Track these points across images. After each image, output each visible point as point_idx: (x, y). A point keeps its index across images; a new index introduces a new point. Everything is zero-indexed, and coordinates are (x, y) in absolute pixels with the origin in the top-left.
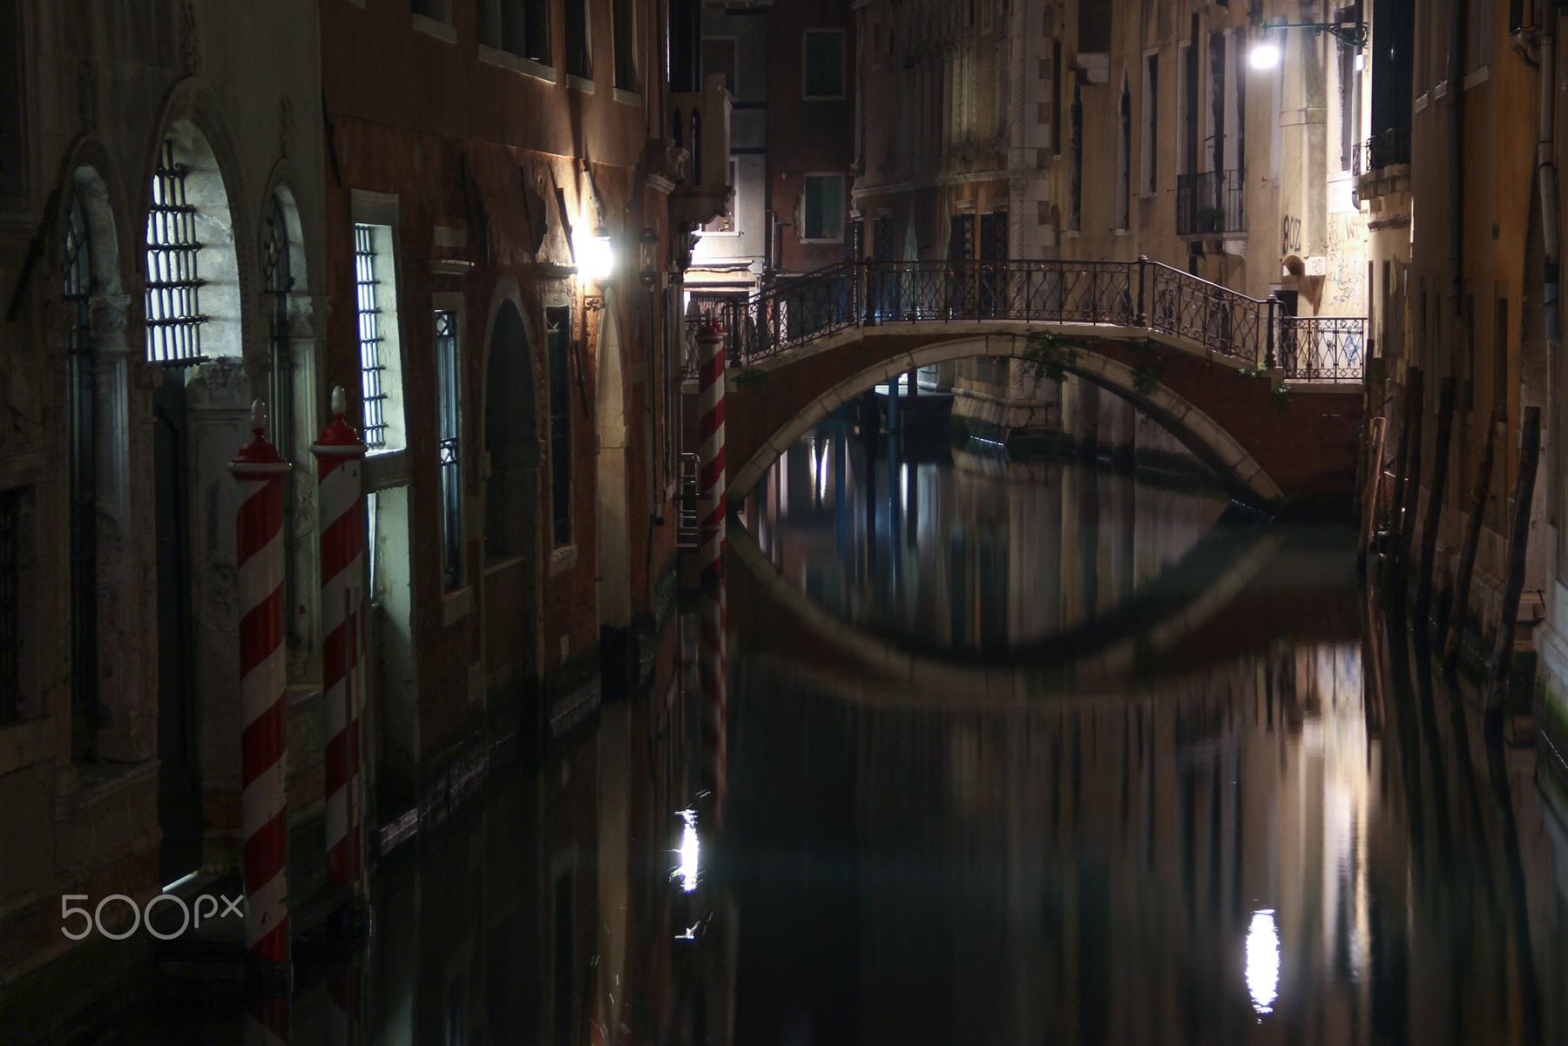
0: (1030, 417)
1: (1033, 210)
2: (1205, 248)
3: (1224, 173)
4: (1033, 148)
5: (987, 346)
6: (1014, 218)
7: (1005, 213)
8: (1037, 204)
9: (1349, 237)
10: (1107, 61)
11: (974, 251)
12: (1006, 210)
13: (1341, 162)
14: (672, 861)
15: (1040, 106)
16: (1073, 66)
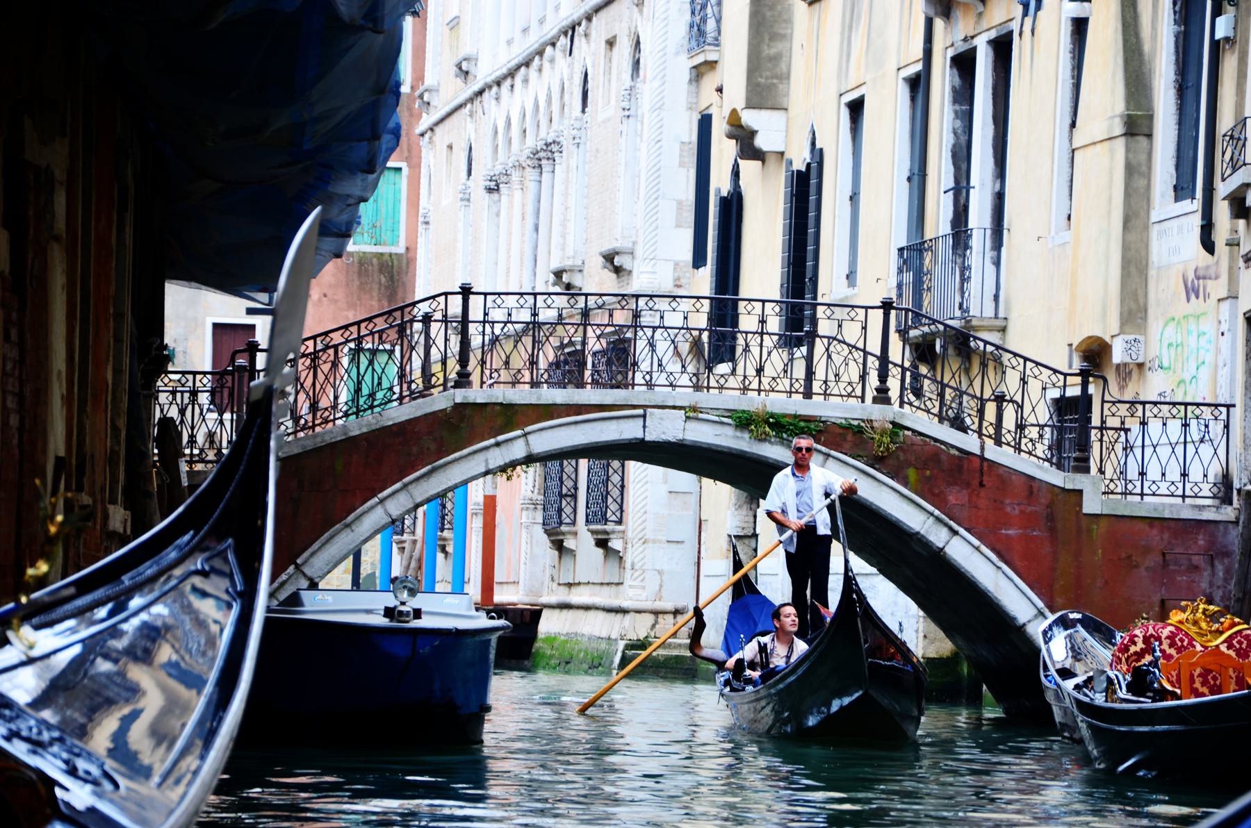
0: (653, 626)
5: (644, 427)
9: (1188, 300)
14: (962, 670)
15: (680, 203)
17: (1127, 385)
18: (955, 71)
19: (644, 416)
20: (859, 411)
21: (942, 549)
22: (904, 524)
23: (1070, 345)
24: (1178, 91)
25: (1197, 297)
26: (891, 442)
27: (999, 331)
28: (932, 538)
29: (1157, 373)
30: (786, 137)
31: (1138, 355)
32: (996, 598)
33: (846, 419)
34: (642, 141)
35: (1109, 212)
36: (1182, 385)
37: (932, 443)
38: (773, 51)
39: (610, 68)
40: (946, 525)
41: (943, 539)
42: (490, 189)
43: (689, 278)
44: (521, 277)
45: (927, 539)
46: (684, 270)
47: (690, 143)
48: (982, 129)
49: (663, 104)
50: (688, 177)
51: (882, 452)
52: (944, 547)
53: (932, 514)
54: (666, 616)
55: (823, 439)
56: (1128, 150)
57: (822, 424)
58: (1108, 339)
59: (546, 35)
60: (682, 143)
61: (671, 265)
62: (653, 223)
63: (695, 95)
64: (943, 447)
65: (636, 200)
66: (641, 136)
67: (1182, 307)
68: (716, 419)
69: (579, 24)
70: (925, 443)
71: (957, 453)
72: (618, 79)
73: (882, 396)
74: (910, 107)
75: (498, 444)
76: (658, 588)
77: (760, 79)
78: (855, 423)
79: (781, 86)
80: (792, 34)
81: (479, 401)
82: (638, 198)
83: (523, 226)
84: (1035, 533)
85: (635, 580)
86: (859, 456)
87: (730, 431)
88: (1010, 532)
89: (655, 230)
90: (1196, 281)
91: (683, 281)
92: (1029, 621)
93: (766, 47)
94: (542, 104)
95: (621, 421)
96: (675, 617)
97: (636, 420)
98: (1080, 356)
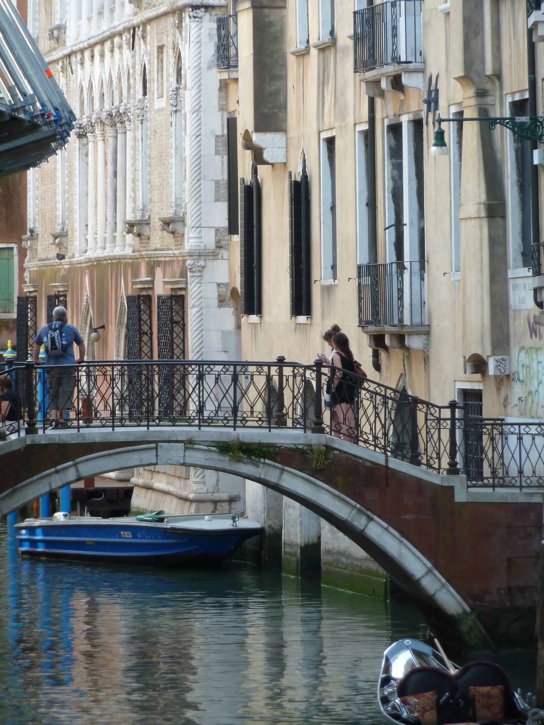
1: (213, 293)
2: (387, 341)
3: (405, 264)
4: (212, 227)
5: (157, 455)
6: (191, 301)
7: (183, 295)
8: (215, 287)
10: (284, 140)
11: (152, 333)
12: (183, 293)
13: (521, 258)
15: (217, 182)
16: (249, 145)
17: (501, 388)
18: (391, 135)
19: (156, 448)
20: (303, 439)
21: (363, 531)
22: (337, 514)
23: (464, 357)
24: (520, 187)
25: (536, 336)
26: (325, 459)
27: (425, 334)
28: (356, 523)
29: (517, 383)
30: (286, 152)
31: (505, 369)
32: (400, 562)
33: (294, 445)
34: (186, 134)
35: (482, 269)
36: (531, 395)
37: (353, 458)
38: (273, 88)
39: (162, 67)
40: (365, 514)
41: (363, 524)
42: (79, 135)
43: (228, 240)
44: (106, 211)
45: (353, 524)
46: (223, 234)
47: (223, 136)
48: (409, 184)
49: (201, 107)
50: (222, 162)
51: (319, 466)
52: (364, 529)
53: (355, 507)
54: (223, 504)
55: (279, 459)
56: (490, 228)
57: (278, 449)
58: (485, 358)
59: (115, 27)
60: (217, 136)
61: (213, 230)
62: (197, 199)
63: (224, 99)
64: (361, 461)
65: (184, 180)
66: (185, 130)
67: (530, 342)
68: (206, 448)
69: (138, 26)
70: (348, 458)
71: (370, 464)
72: (168, 80)
73: (318, 428)
74: (365, 152)
75: (57, 472)
76: (215, 482)
77: (264, 110)
78: (300, 447)
79: (280, 114)
80: (286, 75)
81: (43, 442)
82: (185, 179)
83: (106, 170)
84: (424, 517)
85: (197, 477)
86: (304, 469)
87: (216, 456)
88: (407, 517)
89: (199, 204)
90: (535, 325)
91: (223, 243)
92: (423, 577)
93: (267, 86)
94: (115, 80)
95: (141, 452)
96: (230, 504)
97: (151, 451)
98: (471, 365)
